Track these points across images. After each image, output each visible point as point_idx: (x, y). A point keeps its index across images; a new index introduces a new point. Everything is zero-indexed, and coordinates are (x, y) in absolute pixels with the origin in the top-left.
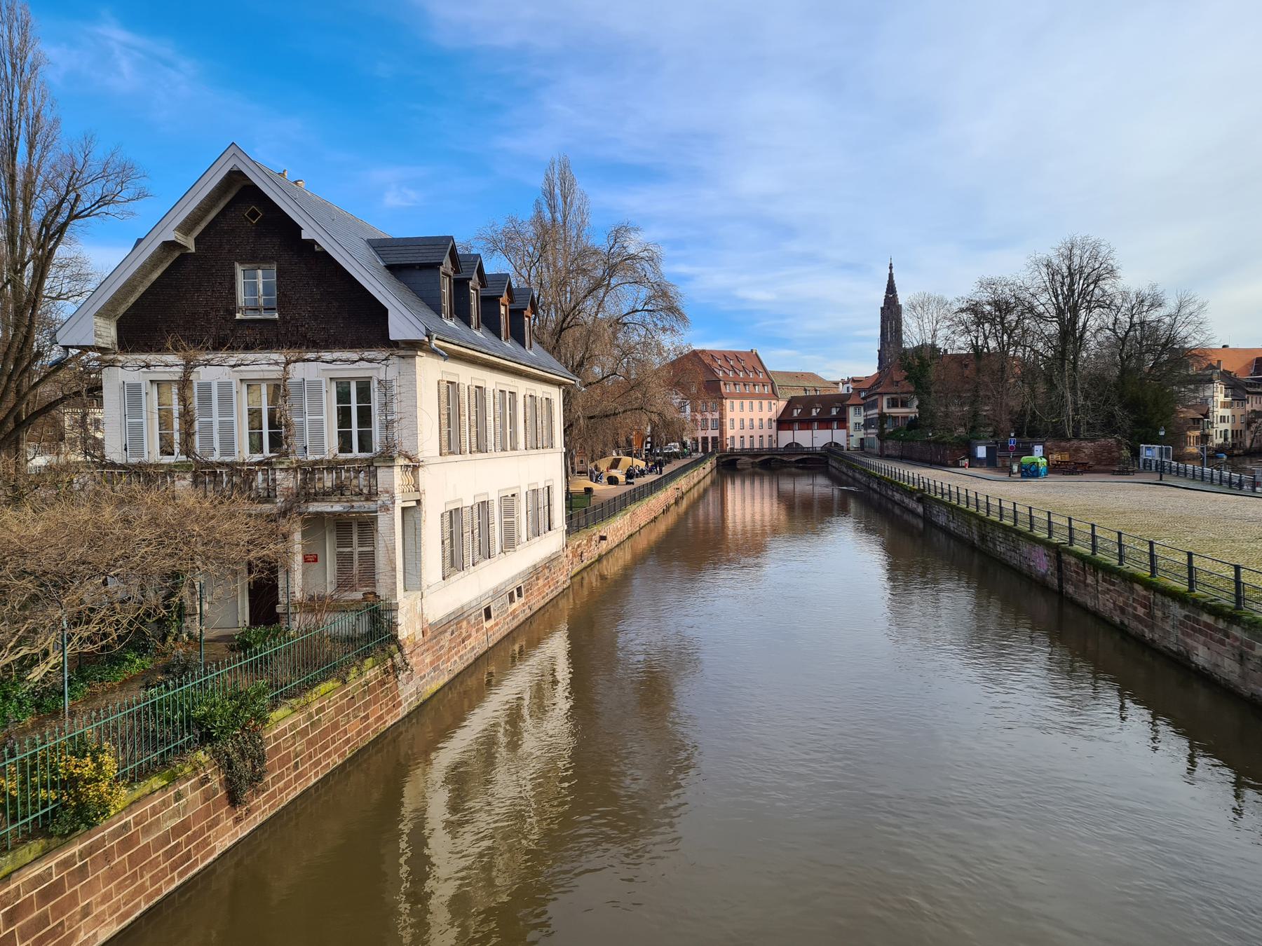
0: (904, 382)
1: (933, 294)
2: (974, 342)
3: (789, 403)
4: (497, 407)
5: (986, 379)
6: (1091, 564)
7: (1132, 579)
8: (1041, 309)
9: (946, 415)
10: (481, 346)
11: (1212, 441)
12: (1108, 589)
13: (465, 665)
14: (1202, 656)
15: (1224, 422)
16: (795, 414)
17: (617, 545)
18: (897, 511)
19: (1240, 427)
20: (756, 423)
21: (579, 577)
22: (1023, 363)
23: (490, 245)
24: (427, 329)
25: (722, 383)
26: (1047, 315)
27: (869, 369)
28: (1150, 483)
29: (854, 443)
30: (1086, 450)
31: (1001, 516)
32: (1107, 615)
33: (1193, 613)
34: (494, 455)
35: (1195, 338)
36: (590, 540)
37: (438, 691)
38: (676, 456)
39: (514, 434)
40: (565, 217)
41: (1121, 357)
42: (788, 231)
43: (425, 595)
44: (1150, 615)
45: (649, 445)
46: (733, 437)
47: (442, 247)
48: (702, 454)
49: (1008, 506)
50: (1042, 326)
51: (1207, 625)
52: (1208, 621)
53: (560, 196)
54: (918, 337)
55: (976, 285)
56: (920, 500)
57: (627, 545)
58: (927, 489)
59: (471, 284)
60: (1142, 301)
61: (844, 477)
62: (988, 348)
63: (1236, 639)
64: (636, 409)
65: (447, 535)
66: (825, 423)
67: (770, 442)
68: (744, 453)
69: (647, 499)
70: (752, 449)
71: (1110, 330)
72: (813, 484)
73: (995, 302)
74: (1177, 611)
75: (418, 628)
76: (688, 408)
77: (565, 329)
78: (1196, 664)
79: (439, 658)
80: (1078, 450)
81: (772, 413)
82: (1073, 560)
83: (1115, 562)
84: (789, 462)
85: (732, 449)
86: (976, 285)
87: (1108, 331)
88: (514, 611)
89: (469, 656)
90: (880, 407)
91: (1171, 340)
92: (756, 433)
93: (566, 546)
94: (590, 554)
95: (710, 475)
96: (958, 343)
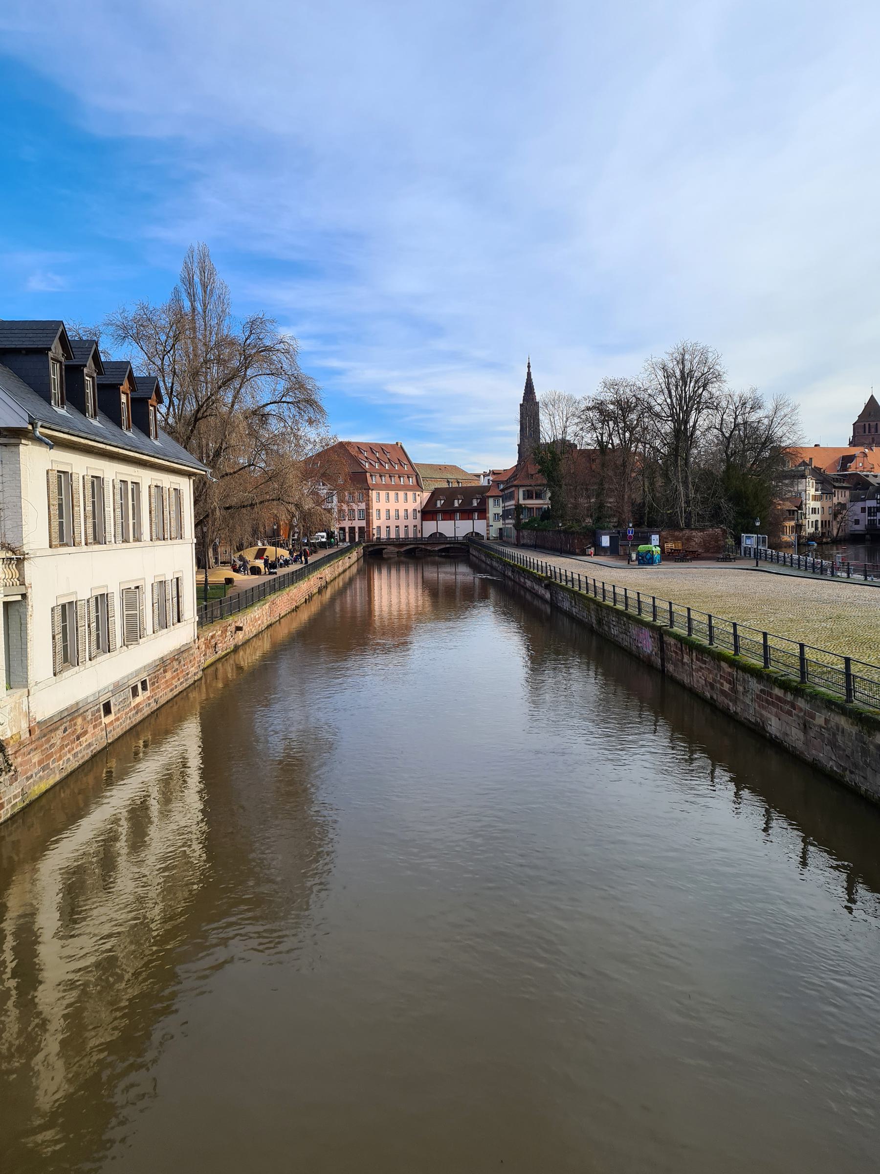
0: (537, 475)
1: (563, 393)
2: (600, 438)
3: (433, 494)
4: (118, 497)
5: (611, 473)
6: (687, 645)
7: (719, 657)
8: (657, 409)
9: (576, 507)
10: (96, 435)
11: (805, 530)
12: (700, 667)
13: (81, 762)
14: (774, 726)
15: (815, 513)
16: (439, 505)
17: (255, 636)
18: (528, 597)
19: (828, 518)
20: (402, 514)
21: (212, 669)
22: (644, 458)
23: (120, 332)
24: (30, 417)
25: (368, 475)
26: (664, 414)
27: (508, 460)
28: (747, 569)
29: (494, 533)
30: (696, 540)
31: (615, 601)
32: (700, 691)
33: (767, 687)
34: (114, 546)
35: (789, 438)
36: (225, 631)
37: (47, 791)
38: (323, 545)
39: (137, 526)
40: (205, 306)
41: (727, 454)
42: (436, 330)
43: (32, 692)
44: (734, 690)
45: (296, 535)
46: (379, 528)
47: (52, 331)
48: (349, 544)
49: (620, 591)
50: (659, 425)
51: (778, 698)
52: (779, 694)
53: (199, 285)
54: (550, 433)
55: (600, 385)
56: (547, 587)
57: (266, 636)
58: (553, 576)
59: (85, 371)
60: (745, 403)
61: (483, 566)
62: (612, 444)
63: (801, 710)
64: (273, 500)
65: (58, 629)
66: (467, 513)
67: (415, 532)
68: (390, 542)
69: (288, 589)
70: (398, 539)
71: (717, 429)
72: (456, 574)
73: (618, 402)
74: (755, 685)
75: (24, 725)
76: (335, 499)
77: (200, 419)
78: (770, 733)
79: (49, 757)
80: (689, 539)
81: (416, 504)
82: (672, 641)
83: (706, 642)
84: (432, 551)
85: (378, 538)
86: (600, 385)
87: (715, 431)
88: (138, 705)
89: (86, 752)
90: (516, 498)
91: (769, 439)
92: (402, 523)
93: (198, 637)
94: (225, 645)
95: (356, 565)
96: (586, 439)
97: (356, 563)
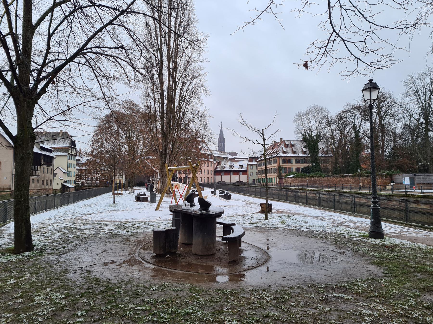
29: (251, 181)
97: (71, 33)
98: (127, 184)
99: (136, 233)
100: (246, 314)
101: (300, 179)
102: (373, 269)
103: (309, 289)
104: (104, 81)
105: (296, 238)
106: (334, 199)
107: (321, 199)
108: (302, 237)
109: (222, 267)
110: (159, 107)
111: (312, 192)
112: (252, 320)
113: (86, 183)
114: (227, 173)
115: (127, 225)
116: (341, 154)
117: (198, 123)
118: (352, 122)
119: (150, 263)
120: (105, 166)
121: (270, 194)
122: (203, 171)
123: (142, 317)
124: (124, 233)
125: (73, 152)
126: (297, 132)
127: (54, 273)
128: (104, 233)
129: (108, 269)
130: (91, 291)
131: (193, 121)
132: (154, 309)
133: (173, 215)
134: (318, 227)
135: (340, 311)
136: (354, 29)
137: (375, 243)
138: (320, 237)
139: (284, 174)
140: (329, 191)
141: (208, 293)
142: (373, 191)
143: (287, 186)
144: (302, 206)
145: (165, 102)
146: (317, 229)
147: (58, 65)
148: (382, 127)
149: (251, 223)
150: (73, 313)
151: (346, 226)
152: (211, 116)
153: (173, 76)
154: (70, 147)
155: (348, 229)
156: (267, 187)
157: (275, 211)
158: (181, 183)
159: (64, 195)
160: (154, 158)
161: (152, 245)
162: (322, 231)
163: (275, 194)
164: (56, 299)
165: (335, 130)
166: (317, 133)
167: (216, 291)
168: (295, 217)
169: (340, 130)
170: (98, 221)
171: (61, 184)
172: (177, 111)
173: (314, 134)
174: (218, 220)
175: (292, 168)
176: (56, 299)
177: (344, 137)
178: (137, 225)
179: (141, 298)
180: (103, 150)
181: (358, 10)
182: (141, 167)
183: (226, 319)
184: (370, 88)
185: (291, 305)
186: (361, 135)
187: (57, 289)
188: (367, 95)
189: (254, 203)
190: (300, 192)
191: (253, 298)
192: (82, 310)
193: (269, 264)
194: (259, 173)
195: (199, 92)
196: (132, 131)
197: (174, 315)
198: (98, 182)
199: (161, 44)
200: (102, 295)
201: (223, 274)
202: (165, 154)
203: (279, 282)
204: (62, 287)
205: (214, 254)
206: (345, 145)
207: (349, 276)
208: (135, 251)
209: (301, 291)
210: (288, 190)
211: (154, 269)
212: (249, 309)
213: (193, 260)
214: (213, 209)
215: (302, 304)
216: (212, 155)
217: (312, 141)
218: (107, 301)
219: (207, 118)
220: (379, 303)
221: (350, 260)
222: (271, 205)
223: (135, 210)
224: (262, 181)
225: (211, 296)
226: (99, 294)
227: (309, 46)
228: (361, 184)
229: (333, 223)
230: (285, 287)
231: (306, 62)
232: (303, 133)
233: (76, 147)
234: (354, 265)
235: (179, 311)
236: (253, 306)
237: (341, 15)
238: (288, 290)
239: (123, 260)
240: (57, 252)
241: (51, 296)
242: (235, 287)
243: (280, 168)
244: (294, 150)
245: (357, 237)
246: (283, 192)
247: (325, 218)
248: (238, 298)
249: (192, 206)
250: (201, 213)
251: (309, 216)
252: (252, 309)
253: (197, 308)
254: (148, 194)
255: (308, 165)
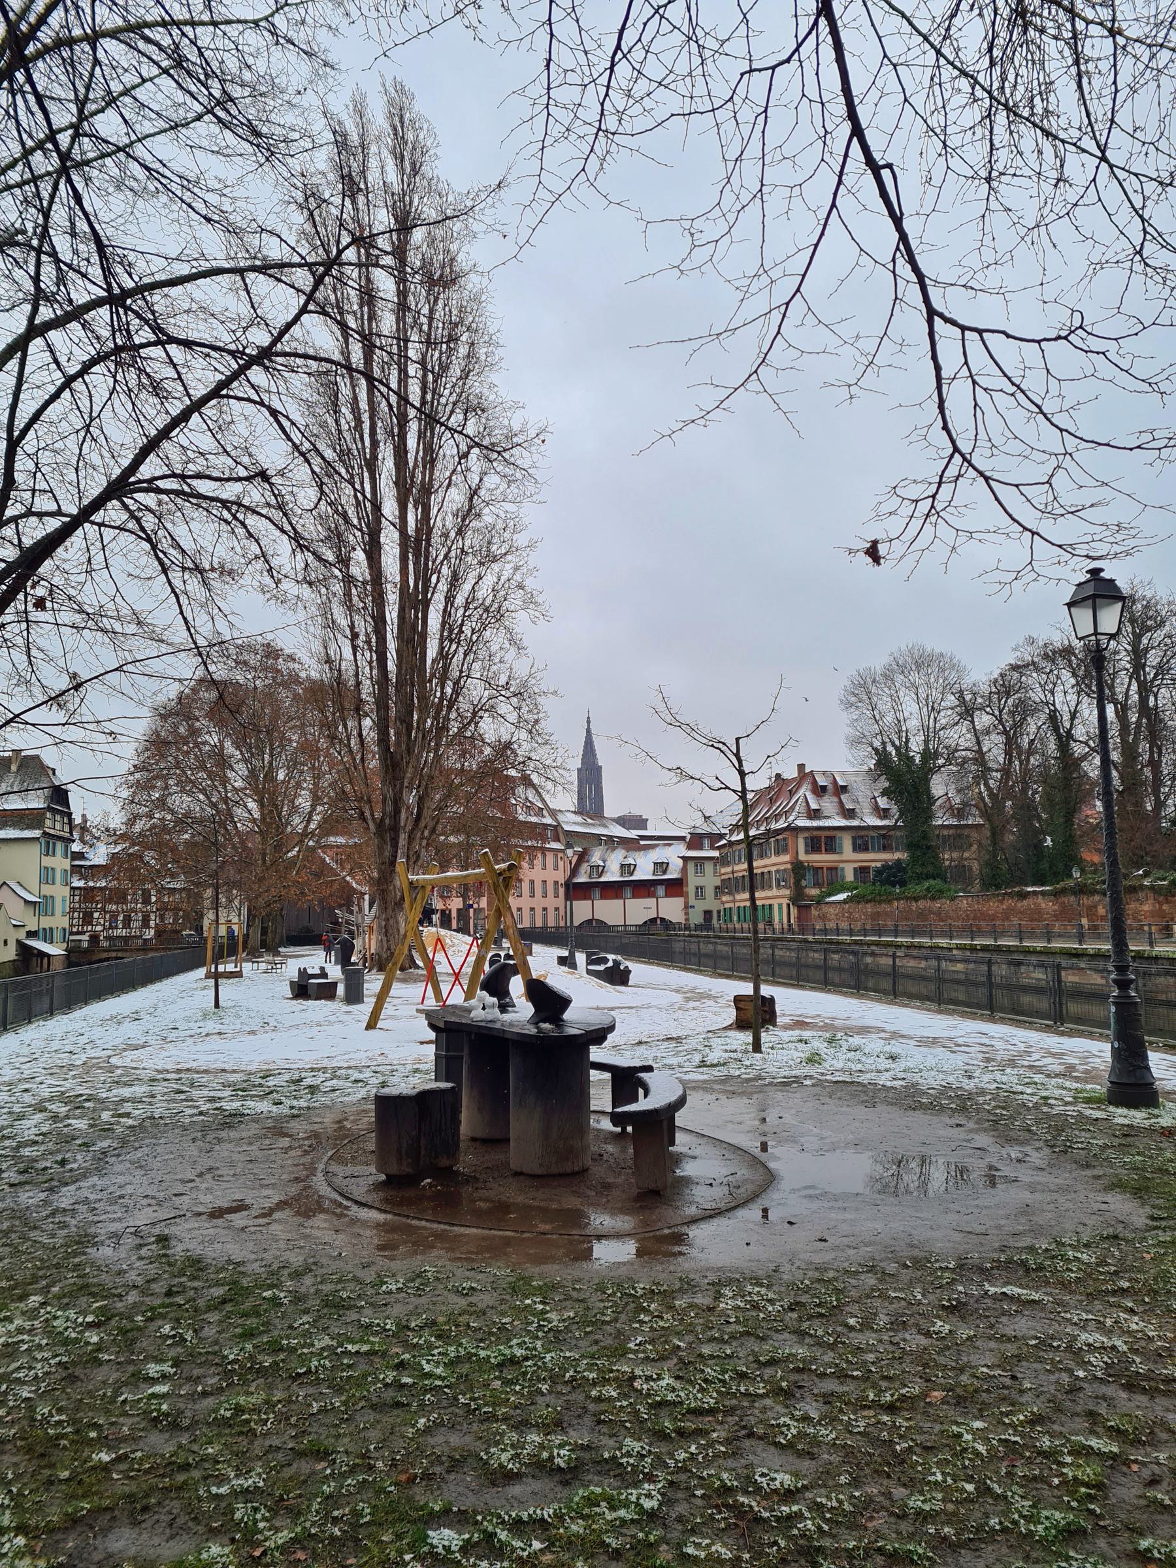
29: (697, 918)
98: (256, 936)
99: (308, 1108)
100: (701, 1356)
101: (869, 908)
102: (1119, 1206)
103: (906, 1275)
104: (193, 584)
105: (861, 1111)
106: (990, 975)
107: (947, 976)
108: (881, 1108)
109: (613, 1212)
110: (370, 663)
111: (915, 952)
112: (724, 1372)
113: (107, 938)
114: (613, 890)
115: (271, 1082)
116: (1013, 817)
117: (508, 717)
118: (1047, 703)
119: (370, 1207)
120: (173, 876)
121: (766, 962)
122: (526, 886)
123: (364, 1376)
124: (265, 1110)
125: (58, 826)
126: (855, 742)
127: (44, 1246)
128: (195, 1111)
129: (228, 1228)
130: (180, 1300)
131: (492, 710)
132: (399, 1350)
133: (437, 1042)
134: (933, 1073)
135: (1007, 1339)
136: (1015, 447)
137: (1126, 1122)
138: (942, 1107)
139: (814, 892)
140: (973, 949)
141: (574, 1294)
142: (1115, 946)
143: (825, 931)
144: (878, 1000)
145: (392, 646)
146: (931, 1081)
147: (39, 534)
148: (1149, 719)
149: (703, 1064)
150: (131, 1369)
151: (1031, 1067)
152: (555, 693)
153: (417, 556)
154: (49, 809)
155: (1038, 1078)
156: (756, 939)
157: (787, 1020)
158: (450, 929)
159: (26, 985)
160: (351, 842)
161: (372, 1146)
162: (948, 1087)
163: (784, 964)
164: (66, 1329)
165: (988, 732)
166: (926, 742)
167: (601, 1288)
168: (856, 1040)
169: (1005, 732)
170: (168, 1072)
171: (19, 942)
172: (433, 675)
173: (916, 746)
174: (596, 1054)
175: (843, 869)
176: (66, 1329)
177: (1019, 754)
178: (308, 1082)
179: (352, 1316)
180: (169, 817)
181: (1023, 392)
182: (305, 876)
183: (638, 1372)
184: (1094, 597)
185: (846, 1325)
186: (1078, 750)
187: (64, 1296)
188: (1084, 617)
189: (710, 997)
190: (873, 954)
191: (722, 1305)
192: (159, 1360)
193: (771, 1199)
194: (727, 887)
195: (512, 608)
196: (272, 750)
197: (467, 1366)
198: (150, 934)
199: (375, 444)
200: (221, 1311)
201: (618, 1236)
202: (395, 829)
203: (806, 1256)
204: (81, 1289)
205: (585, 1170)
206: (1025, 783)
207: (1037, 1231)
208: (312, 1171)
209: (880, 1280)
210: (828, 947)
211: (384, 1224)
212: (712, 1340)
213: (513, 1193)
214: (576, 1017)
215: (883, 1320)
216: (557, 828)
217: (910, 771)
218: (239, 1330)
219: (541, 700)
220: (1132, 1311)
221: (1043, 1180)
222: (771, 1001)
223: (293, 1031)
224: (735, 918)
225: (582, 1306)
226: (209, 1309)
227: (882, 499)
228: (1084, 921)
229: (988, 1060)
230: (826, 1270)
231: (875, 543)
232: (877, 744)
233: (68, 807)
234: (1055, 1196)
235: (483, 1354)
236: (723, 1332)
237: (976, 405)
238: (836, 1279)
239: (276, 1199)
240: (42, 1178)
241: (47, 1320)
242: (662, 1273)
243: (798, 868)
244: (849, 806)
245: (1067, 1103)
246: (811, 954)
247: (960, 1041)
248: (671, 1308)
249: (503, 1008)
250: (540, 1030)
251: (904, 1037)
252: (721, 1341)
253: (539, 1344)
254: (335, 972)
255: (897, 855)
